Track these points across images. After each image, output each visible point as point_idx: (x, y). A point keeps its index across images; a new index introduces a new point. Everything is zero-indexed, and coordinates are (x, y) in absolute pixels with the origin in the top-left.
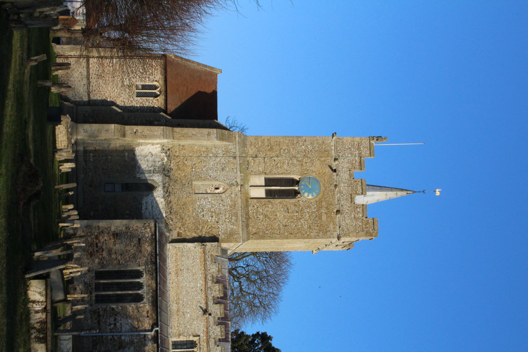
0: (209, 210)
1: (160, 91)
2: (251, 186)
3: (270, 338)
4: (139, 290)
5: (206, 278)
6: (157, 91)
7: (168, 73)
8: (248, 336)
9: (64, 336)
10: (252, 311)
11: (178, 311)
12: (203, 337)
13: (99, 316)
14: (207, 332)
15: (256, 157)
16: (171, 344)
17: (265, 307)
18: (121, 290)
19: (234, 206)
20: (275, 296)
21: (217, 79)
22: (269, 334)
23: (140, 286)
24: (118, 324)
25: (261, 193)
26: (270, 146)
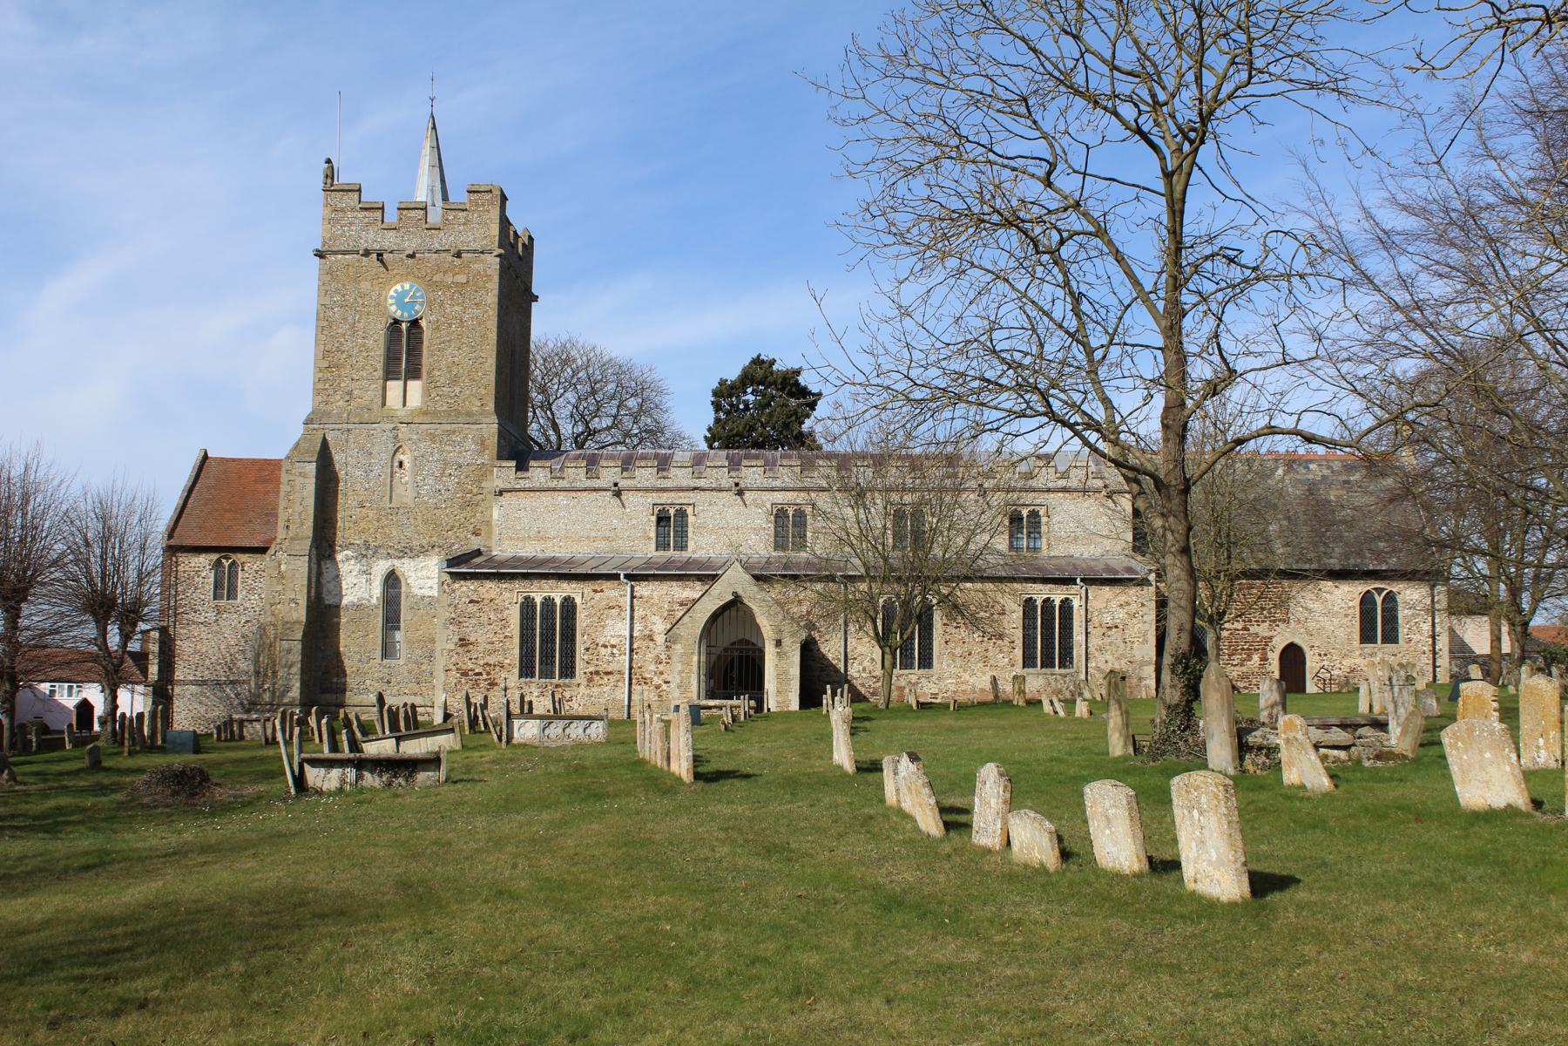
0: (438, 479)
1: (227, 558)
2: (384, 404)
3: (722, 382)
4: (554, 604)
5: (554, 490)
6: (226, 563)
7: (197, 543)
8: (718, 420)
9: (129, 836)
10: (648, 413)
11: (606, 539)
12: (654, 498)
13: (597, 673)
14: (647, 490)
15: (350, 393)
16: (661, 553)
17: (640, 390)
18: (542, 635)
19: (433, 437)
20: (621, 371)
21: (254, 462)
22: (715, 385)
23: (548, 603)
24: (613, 642)
25: (415, 386)
26: (330, 365)
